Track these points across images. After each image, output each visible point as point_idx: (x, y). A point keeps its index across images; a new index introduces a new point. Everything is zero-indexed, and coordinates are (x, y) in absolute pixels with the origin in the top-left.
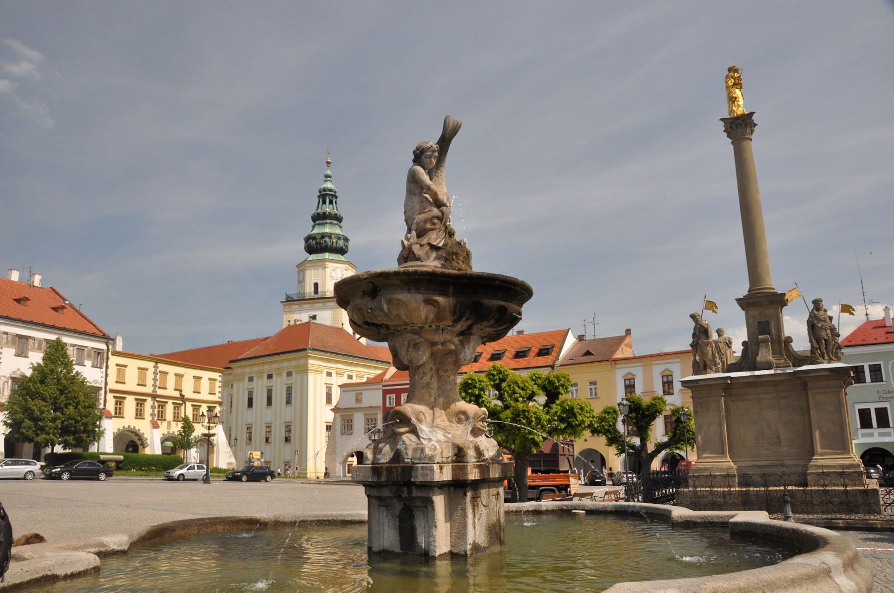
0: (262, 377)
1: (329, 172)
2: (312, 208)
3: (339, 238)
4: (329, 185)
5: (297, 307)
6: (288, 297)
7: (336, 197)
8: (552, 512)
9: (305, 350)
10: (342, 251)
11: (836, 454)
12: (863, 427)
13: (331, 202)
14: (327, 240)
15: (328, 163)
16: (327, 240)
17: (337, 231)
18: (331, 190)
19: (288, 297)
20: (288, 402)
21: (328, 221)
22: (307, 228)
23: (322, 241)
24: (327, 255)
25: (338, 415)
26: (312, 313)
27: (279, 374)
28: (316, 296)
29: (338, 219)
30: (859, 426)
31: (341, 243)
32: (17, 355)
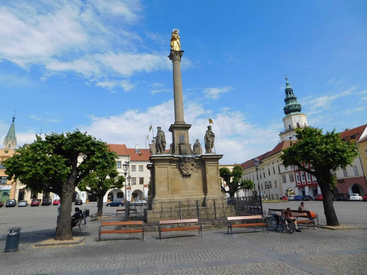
0: (271, 164)
1: (287, 82)
2: (284, 96)
3: (295, 106)
4: (288, 87)
5: (284, 135)
6: (281, 132)
7: (292, 91)
8: (42, 235)
9: (280, 152)
10: (299, 110)
11: (106, 220)
12: (284, 182)
13: (290, 93)
14: (291, 108)
15: (286, 79)
16: (291, 108)
17: (295, 103)
18: (289, 89)
19: (281, 132)
20: (269, 174)
21: (290, 100)
22: (284, 105)
23: (289, 109)
24: (292, 113)
25: (281, 176)
26: (290, 136)
27: (275, 162)
28: (290, 130)
29: (296, 99)
30: (282, 182)
31: (297, 107)
32: (347, 129)
